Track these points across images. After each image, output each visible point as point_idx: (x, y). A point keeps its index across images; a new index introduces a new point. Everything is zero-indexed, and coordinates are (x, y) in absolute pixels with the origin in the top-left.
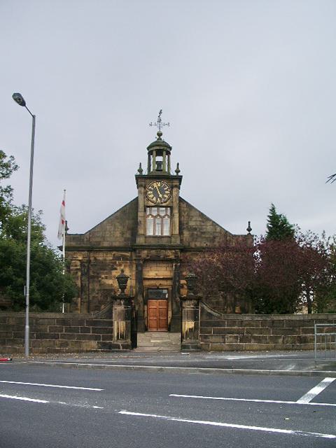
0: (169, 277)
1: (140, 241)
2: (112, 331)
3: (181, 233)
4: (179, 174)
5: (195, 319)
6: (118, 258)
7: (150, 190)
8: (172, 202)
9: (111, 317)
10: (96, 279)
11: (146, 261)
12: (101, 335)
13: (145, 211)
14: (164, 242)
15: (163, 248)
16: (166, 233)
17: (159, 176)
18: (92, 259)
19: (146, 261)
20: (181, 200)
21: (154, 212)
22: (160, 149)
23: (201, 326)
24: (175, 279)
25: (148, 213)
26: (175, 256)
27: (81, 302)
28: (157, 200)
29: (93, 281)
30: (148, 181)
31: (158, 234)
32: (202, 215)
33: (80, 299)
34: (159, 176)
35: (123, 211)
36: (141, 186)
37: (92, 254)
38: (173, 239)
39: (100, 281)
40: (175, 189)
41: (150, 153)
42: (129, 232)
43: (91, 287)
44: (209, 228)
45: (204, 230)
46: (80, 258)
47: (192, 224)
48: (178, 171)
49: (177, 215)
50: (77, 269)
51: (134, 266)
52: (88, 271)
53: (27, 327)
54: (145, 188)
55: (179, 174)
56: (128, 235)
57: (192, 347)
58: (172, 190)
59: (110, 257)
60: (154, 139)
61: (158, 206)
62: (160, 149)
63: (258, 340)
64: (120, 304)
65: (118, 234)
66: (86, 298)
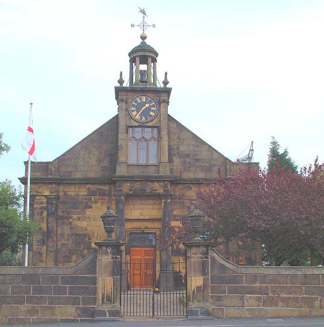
0: (158, 217)
1: (121, 171)
2: (95, 292)
3: (171, 161)
4: (168, 86)
5: (204, 273)
6: (93, 193)
7: (133, 106)
9: (94, 272)
10: (66, 221)
11: (128, 197)
12: (81, 297)
13: (127, 132)
14: (151, 172)
15: (149, 179)
16: (153, 161)
17: (143, 90)
18: (61, 194)
20: (170, 118)
21: (138, 133)
22: (143, 55)
26: (164, 190)
27: (47, 251)
29: (63, 223)
30: (130, 94)
31: (143, 161)
33: (45, 247)
34: (143, 90)
36: (122, 100)
37: (61, 188)
38: (161, 169)
39: (70, 223)
40: (163, 105)
41: (132, 61)
43: (59, 232)
44: (204, 154)
46: (47, 193)
47: (183, 148)
48: (166, 82)
50: (43, 208)
51: (114, 202)
52: (56, 210)
54: (126, 103)
55: (168, 86)
56: (106, 163)
59: (83, 191)
60: (138, 42)
61: (142, 126)
62: (143, 55)
65: (93, 162)
66: (52, 246)
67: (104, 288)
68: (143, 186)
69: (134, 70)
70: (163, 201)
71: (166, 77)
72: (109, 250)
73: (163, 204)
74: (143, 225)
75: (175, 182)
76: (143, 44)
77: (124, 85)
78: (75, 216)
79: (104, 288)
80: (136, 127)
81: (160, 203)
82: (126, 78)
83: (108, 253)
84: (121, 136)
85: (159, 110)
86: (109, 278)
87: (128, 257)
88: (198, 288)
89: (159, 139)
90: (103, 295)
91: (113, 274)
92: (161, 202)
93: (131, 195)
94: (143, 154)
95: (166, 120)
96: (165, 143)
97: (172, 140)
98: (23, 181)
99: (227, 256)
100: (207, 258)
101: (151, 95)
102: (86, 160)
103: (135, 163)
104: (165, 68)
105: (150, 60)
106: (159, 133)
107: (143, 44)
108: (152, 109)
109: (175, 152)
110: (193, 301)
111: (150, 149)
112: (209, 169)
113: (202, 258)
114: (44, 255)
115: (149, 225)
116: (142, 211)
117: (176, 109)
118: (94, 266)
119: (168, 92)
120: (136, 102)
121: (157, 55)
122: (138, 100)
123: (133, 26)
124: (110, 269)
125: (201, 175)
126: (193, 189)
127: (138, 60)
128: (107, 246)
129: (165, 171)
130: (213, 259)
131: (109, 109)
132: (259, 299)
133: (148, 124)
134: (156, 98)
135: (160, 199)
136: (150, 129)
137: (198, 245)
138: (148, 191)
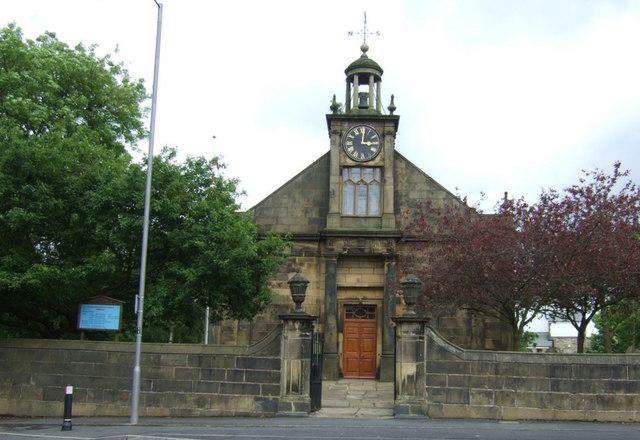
0: (377, 285)
1: (333, 224)
2: (278, 378)
3: (397, 211)
4: (395, 113)
5: (417, 356)
7: (350, 139)
8: (383, 160)
9: (278, 353)
13: (341, 174)
14: (370, 226)
15: (371, 236)
16: (374, 210)
17: (362, 120)
19: (345, 259)
20: (397, 156)
21: (355, 175)
22: (364, 72)
27: (239, 326)
28: (359, 156)
31: (361, 212)
32: (430, 181)
34: (362, 120)
35: (308, 173)
36: (335, 132)
38: (384, 222)
40: (388, 138)
41: (350, 80)
42: (317, 209)
44: (440, 202)
47: (413, 195)
48: (392, 109)
51: (324, 265)
53: (137, 369)
55: (395, 113)
56: (314, 215)
57: (413, 412)
60: (357, 55)
62: (364, 72)
65: (299, 213)
67: (289, 374)
68: (357, 246)
69: (352, 92)
70: (386, 263)
72: (297, 326)
73: (386, 268)
74: (359, 295)
75: (399, 238)
76: (364, 57)
78: (274, 282)
79: (289, 374)
80: (353, 167)
81: (383, 267)
82: (341, 100)
83: (295, 329)
84: (334, 179)
85: (382, 145)
87: (341, 335)
88: (410, 378)
89: (383, 180)
90: (288, 383)
91: (302, 356)
93: (342, 256)
94: (362, 203)
95: (392, 158)
96: (390, 188)
97: (400, 184)
98: (613, 196)
99: (453, 336)
100: (422, 338)
101: (372, 126)
102: (290, 210)
103: (364, 214)
104: (389, 92)
105: (372, 79)
107: (364, 57)
113: (415, 338)
114: (236, 331)
115: (369, 295)
116: (360, 277)
117: (405, 143)
118: (278, 345)
119: (394, 121)
120: (353, 134)
121: (381, 72)
123: (350, 33)
124: (297, 351)
127: (356, 79)
128: (294, 320)
129: (390, 225)
130: (431, 341)
131: (319, 144)
133: (371, 163)
134: (380, 129)
137: (410, 322)
138: (366, 251)
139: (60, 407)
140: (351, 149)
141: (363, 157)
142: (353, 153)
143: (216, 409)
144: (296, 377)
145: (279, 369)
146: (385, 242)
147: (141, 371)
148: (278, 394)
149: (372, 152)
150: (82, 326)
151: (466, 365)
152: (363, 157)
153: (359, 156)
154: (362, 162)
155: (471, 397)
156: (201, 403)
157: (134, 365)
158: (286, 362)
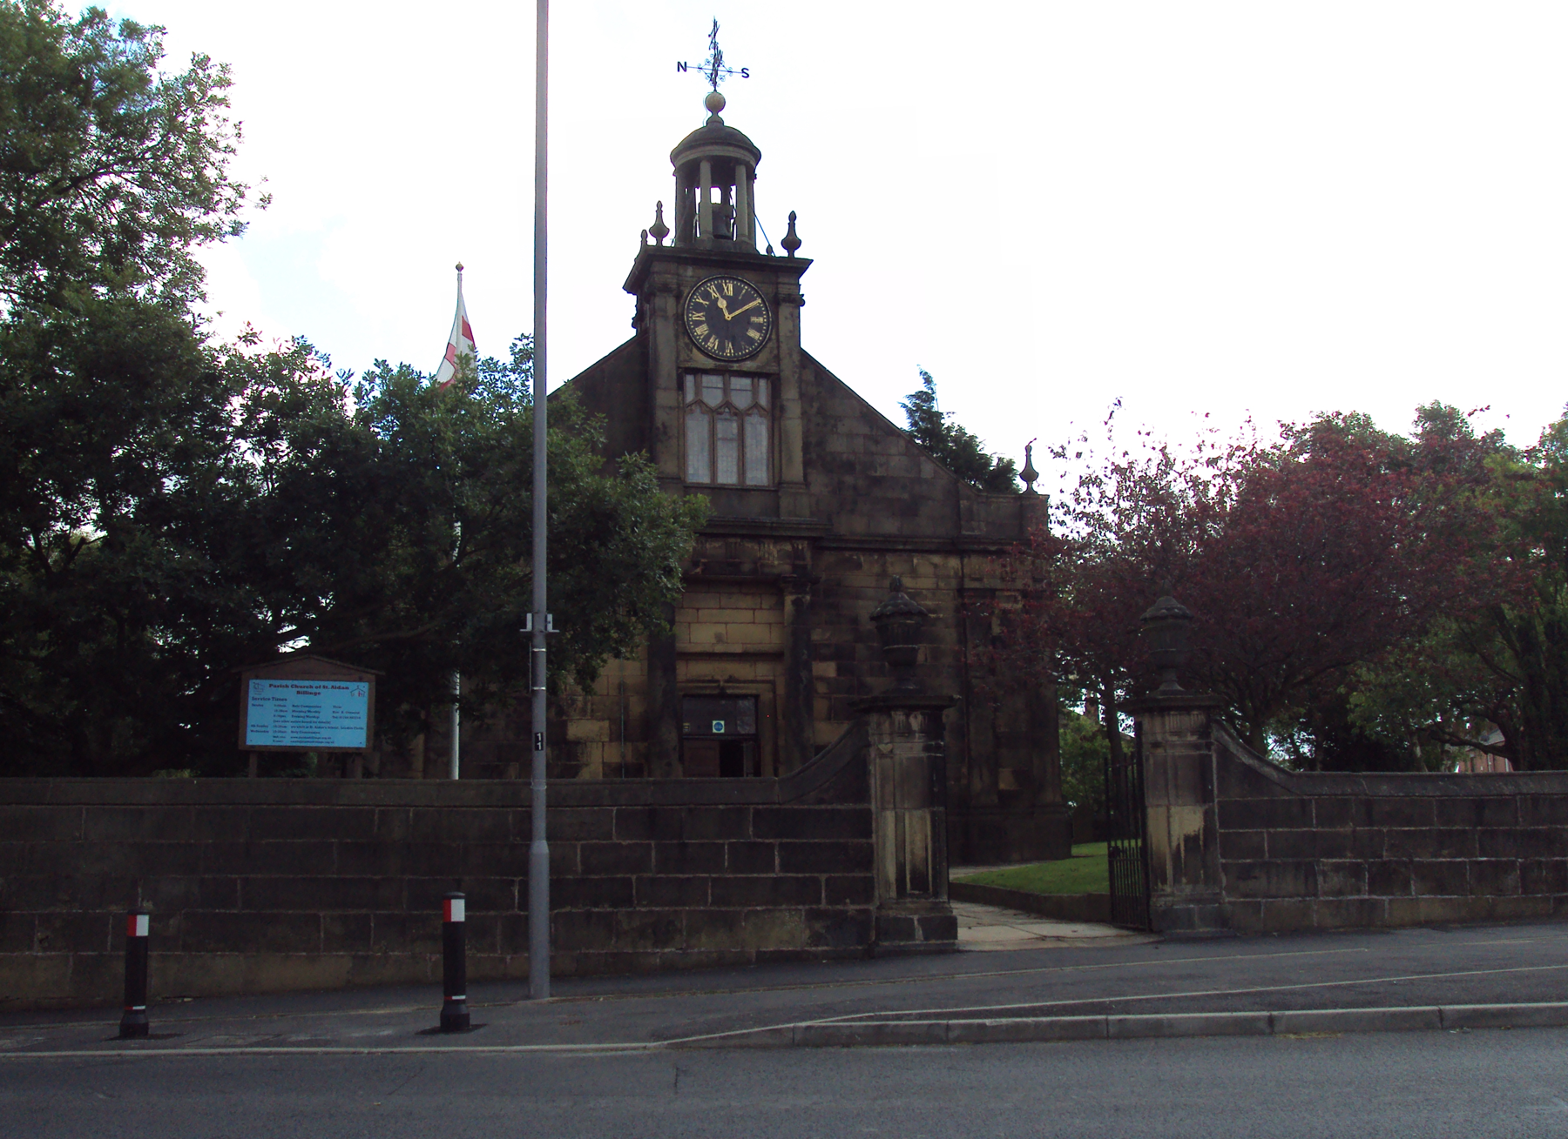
0: (765, 648)
2: (867, 858)
4: (798, 254)
7: (698, 308)
8: (777, 359)
9: (862, 794)
12: (823, 877)
13: (681, 386)
14: (753, 509)
15: (757, 533)
17: (716, 265)
21: (712, 390)
23: (714, 880)
24: (793, 656)
25: (690, 397)
26: (795, 567)
27: (427, 749)
28: (722, 347)
31: (728, 476)
33: (421, 738)
34: (716, 265)
38: (785, 502)
40: (785, 310)
45: (879, 473)
47: (837, 445)
48: (791, 242)
49: (794, 409)
53: (541, 848)
54: (678, 297)
55: (798, 254)
58: (776, 314)
60: (698, 118)
61: (724, 370)
63: (1439, 881)
64: (907, 732)
67: (901, 846)
70: (789, 599)
71: (792, 225)
72: (916, 722)
77: (668, 242)
81: (781, 604)
85: (774, 323)
86: (918, 813)
92: (783, 604)
96: (794, 426)
106: (775, 393)
108: (754, 319)
109: (814, 456)
110: (1176, 881)
111: (749, 441)
112: (909, 510)
113: (1196, 747)
115: (742, 670)
116: (721, 629)
121: (757, 155)
122: (712, 289)
123: (682, 67)
125: (890, 526)
126: (865, 567)
128: (909, 710)
130: (1224, 753)
132: (1355, 871)
133: (749, 365)
135: (780, 595)
136: (746, 382)
138: (747, 567)
139: (432, 960)
140: (702, 330)
141: (729, 350)
142: (707, 339)
143: (706, 945)
144: (920, 853)
145: (869, 835)
146: (788, 547)
147: (551, 854)
148: (869, 898)
149: (751, 341)
150: (254, 739)
151: (1304, 805)
152: (729, 350)
153: (722, 347)
154: (730, 361)
155: (1320, 879)
156: (661, 931)
157: (528, 836)
158: (890, 816)
